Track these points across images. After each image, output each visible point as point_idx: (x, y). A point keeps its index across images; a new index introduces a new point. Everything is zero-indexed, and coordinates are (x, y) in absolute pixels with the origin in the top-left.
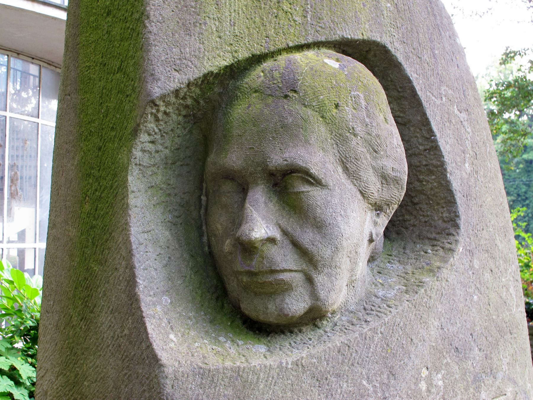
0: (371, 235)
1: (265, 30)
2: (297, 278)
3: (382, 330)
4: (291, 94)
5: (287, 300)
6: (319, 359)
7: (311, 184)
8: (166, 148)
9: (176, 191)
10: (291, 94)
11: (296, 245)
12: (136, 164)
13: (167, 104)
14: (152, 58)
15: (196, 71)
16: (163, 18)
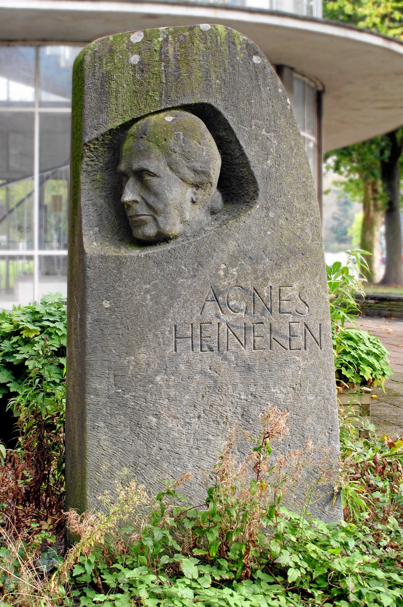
0: (192, 199)
1: (139, 106)
2: (149, 218)
3: (195, 244)
4: (143, 136)
5: (145, 229)
6: (158, 254)
7: (152, 176)
8: (101, 163)
9: (108, 182)
10: (143, 136)
11: (147, 204)
12: (84, 171)
13: (94, 144)
14: (85, 125)
15: (104, 129)
16: (91, 107)
